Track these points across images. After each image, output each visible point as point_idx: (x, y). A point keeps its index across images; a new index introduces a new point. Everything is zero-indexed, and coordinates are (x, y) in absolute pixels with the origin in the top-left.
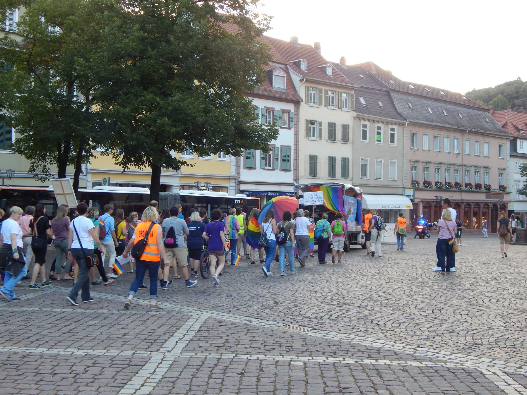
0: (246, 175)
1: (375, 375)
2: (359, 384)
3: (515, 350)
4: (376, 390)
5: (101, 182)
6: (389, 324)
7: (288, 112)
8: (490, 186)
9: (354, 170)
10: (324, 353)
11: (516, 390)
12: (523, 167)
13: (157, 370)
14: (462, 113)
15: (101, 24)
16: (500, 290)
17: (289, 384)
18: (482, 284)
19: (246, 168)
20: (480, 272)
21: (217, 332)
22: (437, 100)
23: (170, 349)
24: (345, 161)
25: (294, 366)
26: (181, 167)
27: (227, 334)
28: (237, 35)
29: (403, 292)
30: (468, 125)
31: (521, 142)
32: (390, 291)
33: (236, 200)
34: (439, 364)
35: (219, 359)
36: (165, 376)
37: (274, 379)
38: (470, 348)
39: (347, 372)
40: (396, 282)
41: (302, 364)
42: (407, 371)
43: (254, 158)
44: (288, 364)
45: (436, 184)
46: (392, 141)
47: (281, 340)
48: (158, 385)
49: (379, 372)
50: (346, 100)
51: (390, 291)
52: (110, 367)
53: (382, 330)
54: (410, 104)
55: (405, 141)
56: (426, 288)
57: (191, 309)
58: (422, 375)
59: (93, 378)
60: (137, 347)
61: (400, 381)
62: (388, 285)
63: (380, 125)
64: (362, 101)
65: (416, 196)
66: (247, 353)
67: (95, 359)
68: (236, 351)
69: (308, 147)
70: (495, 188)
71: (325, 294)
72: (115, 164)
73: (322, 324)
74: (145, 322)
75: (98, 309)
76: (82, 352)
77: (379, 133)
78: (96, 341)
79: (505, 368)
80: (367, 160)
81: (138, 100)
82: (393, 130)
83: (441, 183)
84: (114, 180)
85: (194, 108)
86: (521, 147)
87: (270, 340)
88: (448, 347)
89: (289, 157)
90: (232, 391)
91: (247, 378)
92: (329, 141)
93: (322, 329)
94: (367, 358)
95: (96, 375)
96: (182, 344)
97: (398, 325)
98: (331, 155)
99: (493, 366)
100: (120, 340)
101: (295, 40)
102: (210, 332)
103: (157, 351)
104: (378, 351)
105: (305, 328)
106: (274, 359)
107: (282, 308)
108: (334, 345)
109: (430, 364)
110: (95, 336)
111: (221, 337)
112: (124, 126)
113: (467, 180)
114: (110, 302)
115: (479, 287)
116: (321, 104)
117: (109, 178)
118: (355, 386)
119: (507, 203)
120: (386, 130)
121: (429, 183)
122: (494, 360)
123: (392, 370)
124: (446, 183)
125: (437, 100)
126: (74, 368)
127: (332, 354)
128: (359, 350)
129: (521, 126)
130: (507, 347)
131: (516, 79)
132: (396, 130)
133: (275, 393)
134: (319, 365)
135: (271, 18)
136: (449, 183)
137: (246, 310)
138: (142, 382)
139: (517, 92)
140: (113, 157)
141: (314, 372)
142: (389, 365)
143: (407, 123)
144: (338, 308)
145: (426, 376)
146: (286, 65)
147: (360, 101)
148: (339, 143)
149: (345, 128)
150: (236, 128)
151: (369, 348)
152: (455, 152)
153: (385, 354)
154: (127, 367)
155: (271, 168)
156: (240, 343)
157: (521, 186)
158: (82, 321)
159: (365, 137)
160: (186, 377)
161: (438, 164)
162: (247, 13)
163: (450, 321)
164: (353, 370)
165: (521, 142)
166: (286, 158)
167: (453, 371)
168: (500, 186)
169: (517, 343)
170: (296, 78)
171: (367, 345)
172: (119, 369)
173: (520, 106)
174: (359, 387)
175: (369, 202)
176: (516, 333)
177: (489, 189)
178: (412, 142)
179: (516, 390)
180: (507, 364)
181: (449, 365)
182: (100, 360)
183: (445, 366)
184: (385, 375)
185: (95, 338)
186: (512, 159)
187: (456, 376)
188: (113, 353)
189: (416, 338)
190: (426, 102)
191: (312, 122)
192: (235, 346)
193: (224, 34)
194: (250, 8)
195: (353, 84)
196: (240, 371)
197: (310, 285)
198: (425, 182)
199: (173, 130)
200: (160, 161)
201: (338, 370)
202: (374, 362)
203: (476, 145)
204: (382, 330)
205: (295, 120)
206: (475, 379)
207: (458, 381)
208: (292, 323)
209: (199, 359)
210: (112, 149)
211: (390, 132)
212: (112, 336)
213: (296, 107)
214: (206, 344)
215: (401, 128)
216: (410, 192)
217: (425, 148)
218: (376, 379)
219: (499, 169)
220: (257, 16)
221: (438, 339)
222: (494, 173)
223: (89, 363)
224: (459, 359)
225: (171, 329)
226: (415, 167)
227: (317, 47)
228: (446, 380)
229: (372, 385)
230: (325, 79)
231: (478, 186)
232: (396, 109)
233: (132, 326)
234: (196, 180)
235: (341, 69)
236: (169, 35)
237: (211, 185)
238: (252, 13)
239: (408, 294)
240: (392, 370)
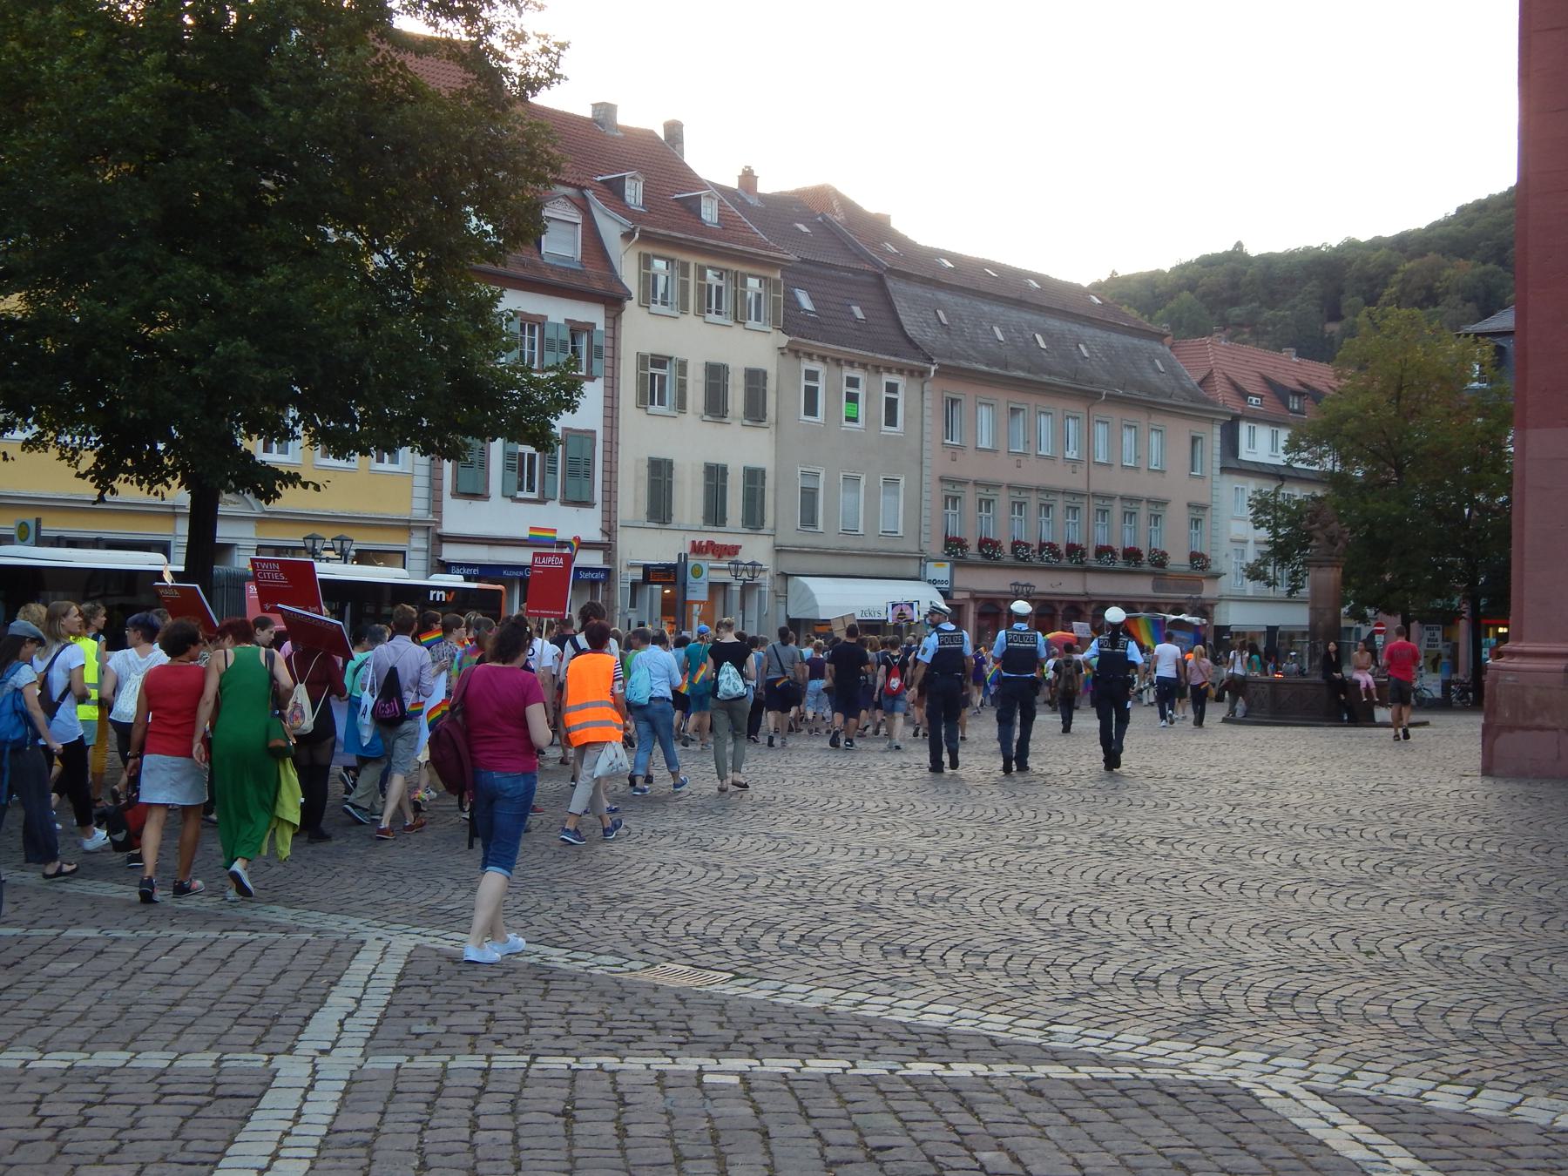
0: (459, 517)
1: (955, 1107)
2: (920, 1136)
3: (1324, 1026)
4: (971, 1150)
5: (12, 532)
6: (954, 958)
7: (589, 328)
8: (1164, 554)
9: (781, 507)
10: (789, 1047)
11: (1357, 1140)
12: (1258, 502)
13: (306, 1108)
14: (1089, 345)
15: (41, 44)
16: (1242, 855)
17: (715, 1140)
18: (1189, 838)
19: (458, 494)
20: (1174, 805)
21: (455, 990)
22: (1020, 303)
23: (328, 1046)
24: (754, 477)
25: (715, 1087)
26: (284, 492)
27: (489, 997)
28: (458, 96)
29: (970, 864)
30: (1106, 378)
31: (1252, 431)
32: (934, 862)
33: (432, 593)
34: (1125, 1072)
35: (486, 1072)
36: (337, 1126)
37: (667, 1128)
38: (1200, 1024)
39: (875, 1103)
40: (944, 833)
41: (735, 1080)
42: (1041, 1094)
43: (484, 465)
44: (695, 1082)
45: (1014, 550)
46: (891, 420)
47: (653, 1011)
48: (323, 1154)
49: (964, 1099)
50: (759, 296)
51: (934, 862)
52: (157, 1102)
53: (939, 976)
54: (941, 313)
55: (927, 420)
56: (1035, 852)
57: (354, 922)
58: (1088, 1104)
59: (113, 1138)
60: (224, 1039)
61: (1031, 1123)
62: (923, 843)
63: (857, 373)
64: (805, 301)
65: (956, 584)
66: (565, 1052)
67: (104, 1078)
68: (531, 1047)
69: (646, 435)
70: (1178, 560)
71: (746, 872)
73: (760, 960)
74: (224, 963)
75: (66, 928)
76: (54, 1061)
77: (852, 398)
78: (91, 1026)
79: (1307, 1078)
80: (817, 475)
81: (157, 284)
82: (892, 388)
83: (1027, 546)
84: (51, 527)
85: (330, 312)
86: (1252, 444)
87: (621, 1012)
88: (1138, 1022)
89: (590, 462)
90: (551, 1165)
91: (587, 1125)
92: (707, 418)
93: (762, 975)
94: (918, 1058)
95: (121, 1130)
96: (360, 1027)
97: (980, 961)
98: (714, 460)
99: (1274, 1073)
100: (162, 1020)
101: (605, 112)
102: (434, 989)
103: (290, 1050)
104: (944, 1037)
105: (712, 973)
106: (648, 1066)
107: (631, 916)
108: (812, 1022)
109: (1102, 1072)
110: (83, 1008)
111: (473, 1007)
112: (109, 362)
113: (1101, 537)
114: (95, 902)
115: (1181, 847)
116: (684, 308)
117: (38, 521)
118: (906, 1141)
119: (1212, 606)
120: (872, 388)
121: (996, 545)
122: (1274, 1055)
123: (997, 1091)
124: (1042, 546)
125: (1020, 303)
126: (45, 1110)
127: (813, 1049)
128: (890, 1037)
129: (1251, 384)
130: (1299, 1017)
131: (1230, 249)
132: (901, 390)
133: (681, 1170)
134: (786, 1083)
135: (563, 46)
136: (1052, 546)
137: (523, 923)
138: (272, 1148)
139: (1235, 286)
140: (62, 457)
141: (778, 1104)
142: (986, 1077)
144: (797, 914)
145: (1098, 1106)
146: (581, 188)
147: (797, 302)
148: (737, 424)
149: (755, 378)
150: (453, 375)
151: (915, 1030)
152: (1068, 455)
153: (965, 1046)
154: (210, 1103)
155: (534, 496)
156: (535, 1023)
157: (1251, 556)
158: (26, 965)
159: (811, 409)
160: (399, 1127)
161: (1020, 489)
162: (489, 30)
163: (1125, 946)
164: (890, 1095)
165: (1252, 431)
166: (579, 469)
167: (1172, 1090)
168: (1194, 557)
169: (1326, 1006)
170: (610, 229)
171: (906, 1020)
172: (189, 1110)
173: (1240, 325)
174: (920, 1143)
175: (821, 601)
176: (1314, 976)
177: (1162, 564)
178: (948, 423)
179: (1357, 1140)
180: (1313, 1068)
181: (1153, 1073)
182: (120, 1084)
183: (1143, 1076)
184: (983, 1107)
185: (83, 1016)
186: (1226, 477)
187: (1183, 1104)
188: (155, 1060)
189: (1041, 997)
190: (986, 308)
191: (660, 361)
192: (522, 1031)
193: (414, 88)
194: (499, 15)
195: (778, 251)
196: (560, 1107)
197: (696, 848)
198: (983, 543)
199: (266, 375)
200: (217, 473)
201: (847, 1097)
202: (940, 1070)
203: (1128, 437)
204: (939, 976)
205: (609, 352)
206: (1237, 1111)
207: (1192, 1118)
208: (670, 960)
209: (424, 1074)
210: (58, 433)
211: (885, 395)
212: (134, 1008)
213: (612, 314)
214: (433, 1028)
215: (915, 384)
216: (941, 572)
217: (985, 443)
218: (963, 1119)
219: (1189, 505)
220: (521, 38)
221: (1103, 997)
222: (1176, 515)
223: (90, 1091)
224: (1175, 1055)
225: (311, 984)
226: (955, 499)
227: (674, 131)
228: (1157, 1117)
229: (957, 1138)
230: (696, 234)
231: (1132, 554)
232: (901, 327)
233: (187, 976)
234: (309, 531)
235: (744, 206)
236: (254, 88)
237: (354, 547)
238: (504, 30)
239: (986, 869)
240: (997, 1091)
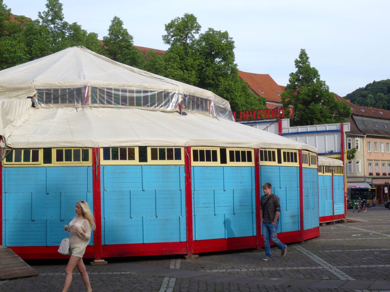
72: (40, 13)
143: (365, 136)
161: (377, 160)
